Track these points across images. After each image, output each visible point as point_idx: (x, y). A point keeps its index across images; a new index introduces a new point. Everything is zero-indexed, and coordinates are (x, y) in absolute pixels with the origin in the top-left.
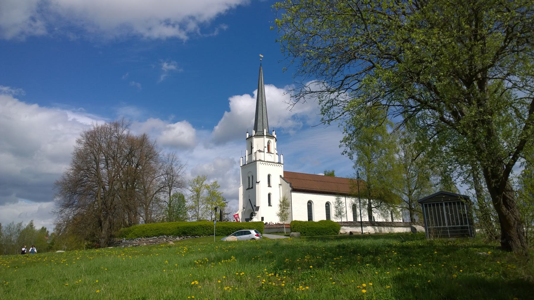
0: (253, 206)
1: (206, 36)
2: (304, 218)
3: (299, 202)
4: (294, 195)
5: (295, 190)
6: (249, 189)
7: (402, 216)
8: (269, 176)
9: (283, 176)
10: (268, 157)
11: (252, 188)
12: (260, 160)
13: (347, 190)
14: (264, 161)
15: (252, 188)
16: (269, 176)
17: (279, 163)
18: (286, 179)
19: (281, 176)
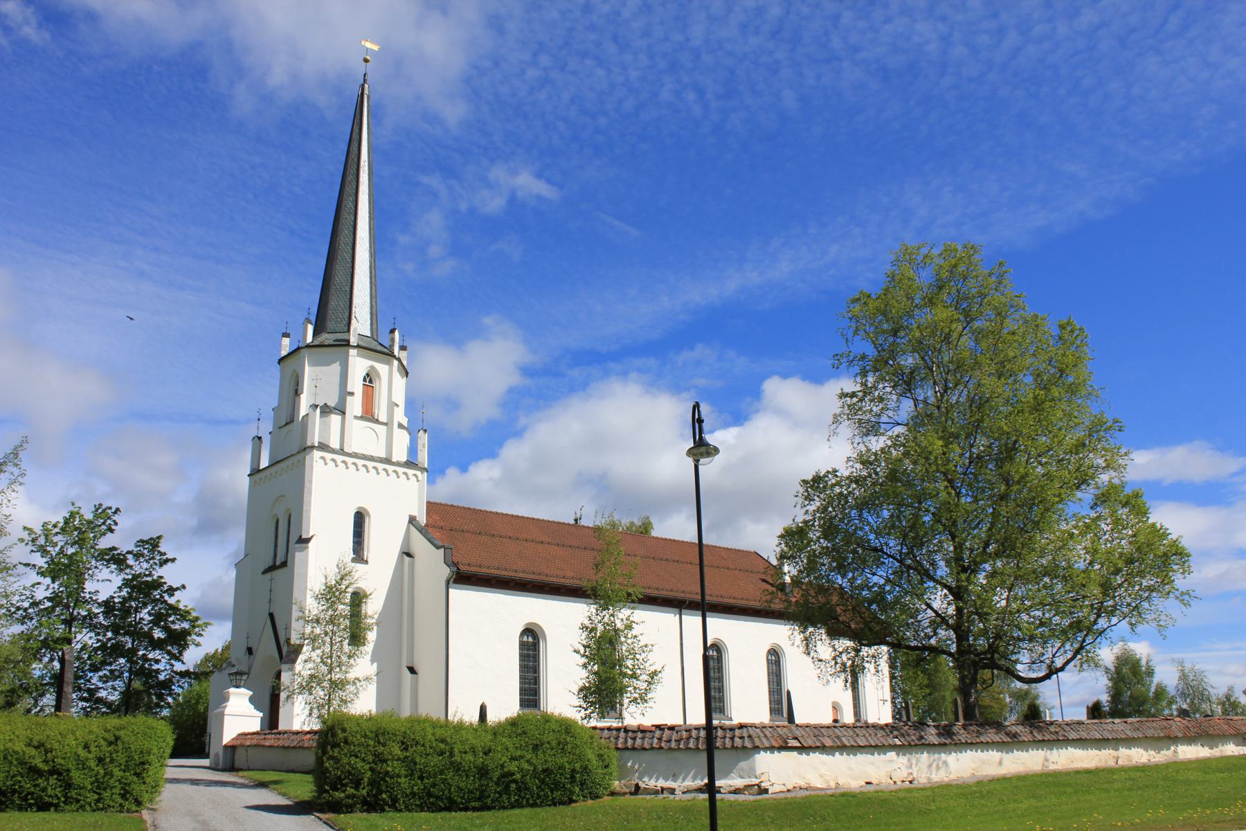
0: (282, 640)
1: (372, 636)
2: (505, 705)
3: (485, 626)
4: (461, 597)
5: (463, 578)
6: (272, 568)
7: (862, 645)
8: (360, 519)
9: (422, 520)
10: (363, 437)
11: (284, 564)
12: (323, 447)
13: (753, 593)
14: (341, 451)
15: (284, 564)
16: (360, 519)
17: (410, 464)
18: (436, 534)
19: (412, 520)
